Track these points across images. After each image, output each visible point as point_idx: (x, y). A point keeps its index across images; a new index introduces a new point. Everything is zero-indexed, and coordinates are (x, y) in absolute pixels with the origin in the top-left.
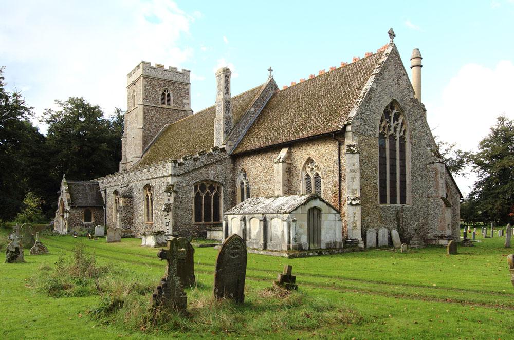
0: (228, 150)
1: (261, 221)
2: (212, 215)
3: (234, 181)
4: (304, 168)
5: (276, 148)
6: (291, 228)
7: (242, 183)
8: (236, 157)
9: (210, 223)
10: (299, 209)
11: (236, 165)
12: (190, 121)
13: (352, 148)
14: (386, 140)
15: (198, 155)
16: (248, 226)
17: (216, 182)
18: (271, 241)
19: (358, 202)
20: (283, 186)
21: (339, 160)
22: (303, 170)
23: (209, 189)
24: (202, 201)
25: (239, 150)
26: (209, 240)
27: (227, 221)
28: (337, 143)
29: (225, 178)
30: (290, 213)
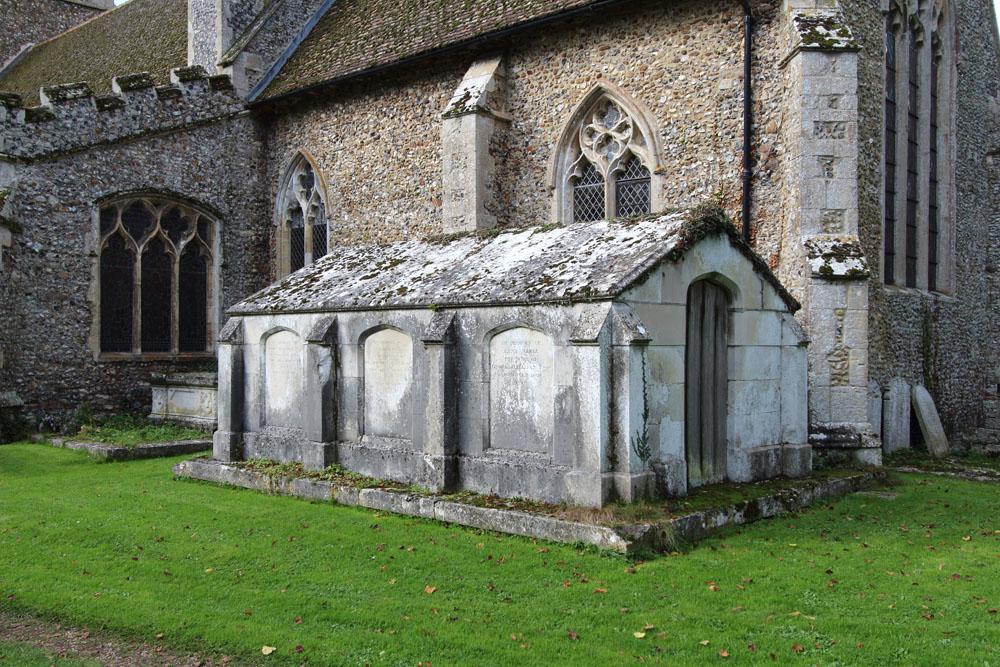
0: (242, 87)
1: (428, 342)
2: (176, 327)
3: (265, 205)
4: (571, 137)
5: (441, 64)
6: (625, 380)
7: (296, 211)
8: (274, 113)
9: (168, 356)
10: (654, 281)
11: (271, 144)
12: (106, 26)
13: (821, 29)
14: (898, 37)
15: (117, 89)
16: (350, 370)
17: (192, 201)
18: (487, 445)
19: (855, 264)
20: (478, 211)
21: (749, 91)
22: (563, 145)
23: (164, 226)
24: (132, 271)
25: (287, 86)
26: (159, 423)
27: (242, 343)
28: (737, 21)
29: (231, 189)
30: (615, 296)
